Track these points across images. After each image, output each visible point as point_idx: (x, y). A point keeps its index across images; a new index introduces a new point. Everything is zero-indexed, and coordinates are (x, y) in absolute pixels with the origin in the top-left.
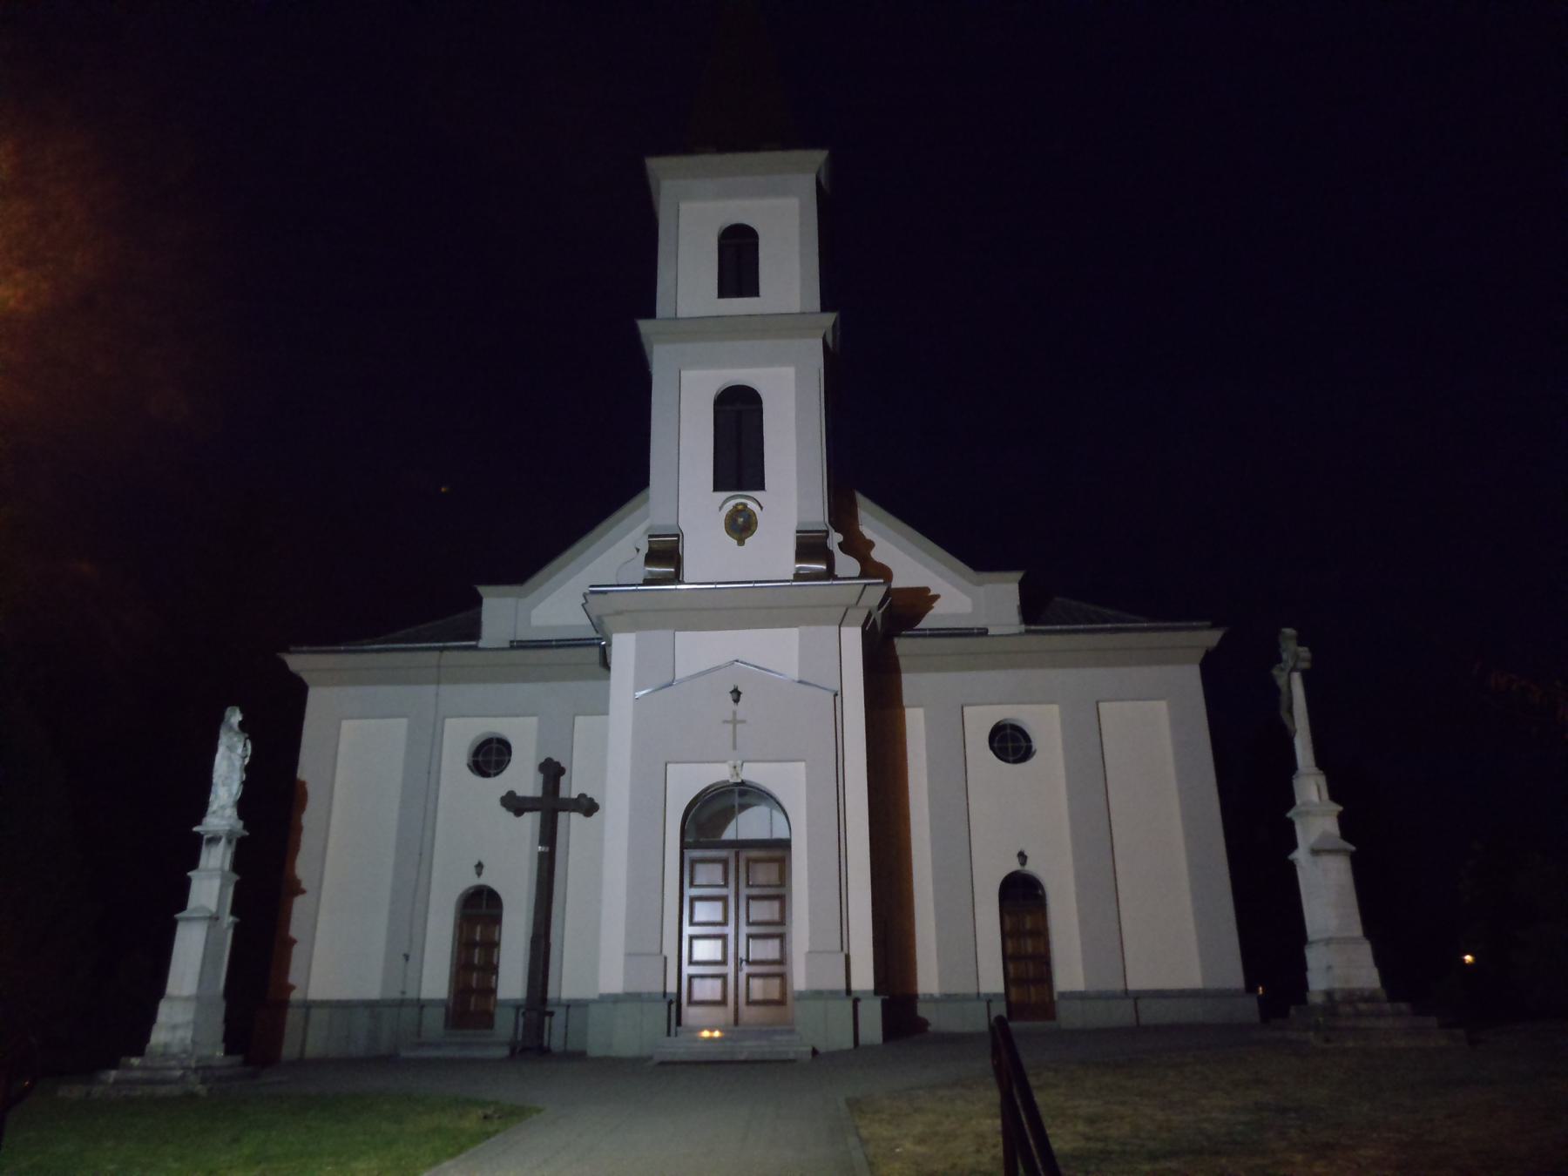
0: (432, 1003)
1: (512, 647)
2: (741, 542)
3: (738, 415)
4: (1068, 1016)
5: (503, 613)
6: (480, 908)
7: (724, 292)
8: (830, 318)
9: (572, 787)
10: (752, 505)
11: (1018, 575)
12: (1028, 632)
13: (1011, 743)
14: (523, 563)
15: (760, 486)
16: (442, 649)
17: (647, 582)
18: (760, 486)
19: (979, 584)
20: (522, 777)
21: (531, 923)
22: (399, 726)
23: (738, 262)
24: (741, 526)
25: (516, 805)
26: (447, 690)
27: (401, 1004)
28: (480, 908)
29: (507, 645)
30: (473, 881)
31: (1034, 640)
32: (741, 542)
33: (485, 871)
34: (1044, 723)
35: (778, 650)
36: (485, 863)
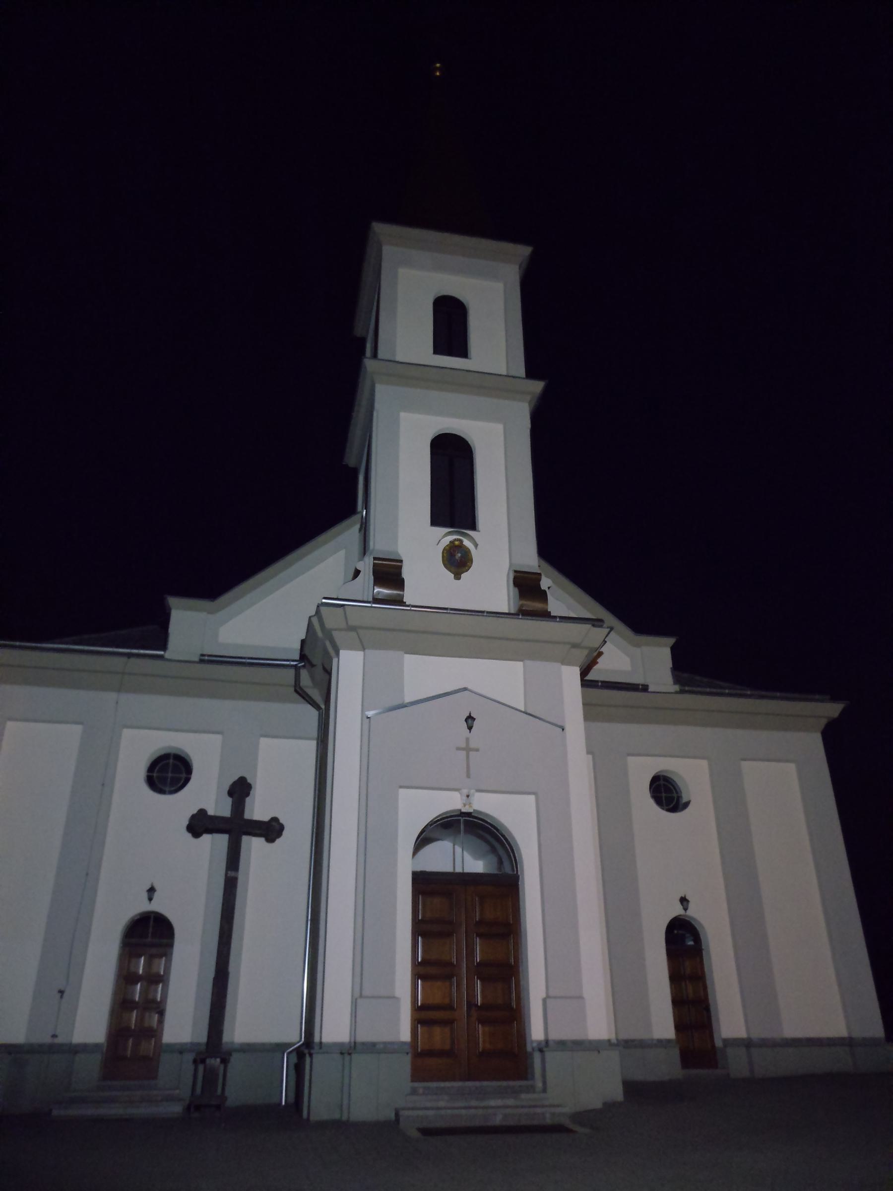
0: (84, 1048)
1: (202, 661)
2: (457, 577)
3: (452, 462)
4: (737, 1065)
5: (192, 626)
6: (149, 934)
7: (437, 350)
8: (538, 386)
9: (258, 809)
10: (467, 543)
11: (671, 641)
12: (682, 692)
13: (666, 793)
14: (222, 572)
15: (473, 526)
16: (129, 655)
17: (376, 600)
18: (473, 526)
19: (638, 645)
20: (205, 793)
21: (527, 972)
22: (71, 734)
23: (451, 326)
24: (457, 561)
25: (200, 824)
26: (126, 699)
27: (52, 1049)
28: (149, 934)
29: (197, 659)
30: (143, 906)
31: (689, 700)
32: (457, 577)
33: (156, 896)
34: (693, 776)
35: (501, 679)
36: (156, 887)
